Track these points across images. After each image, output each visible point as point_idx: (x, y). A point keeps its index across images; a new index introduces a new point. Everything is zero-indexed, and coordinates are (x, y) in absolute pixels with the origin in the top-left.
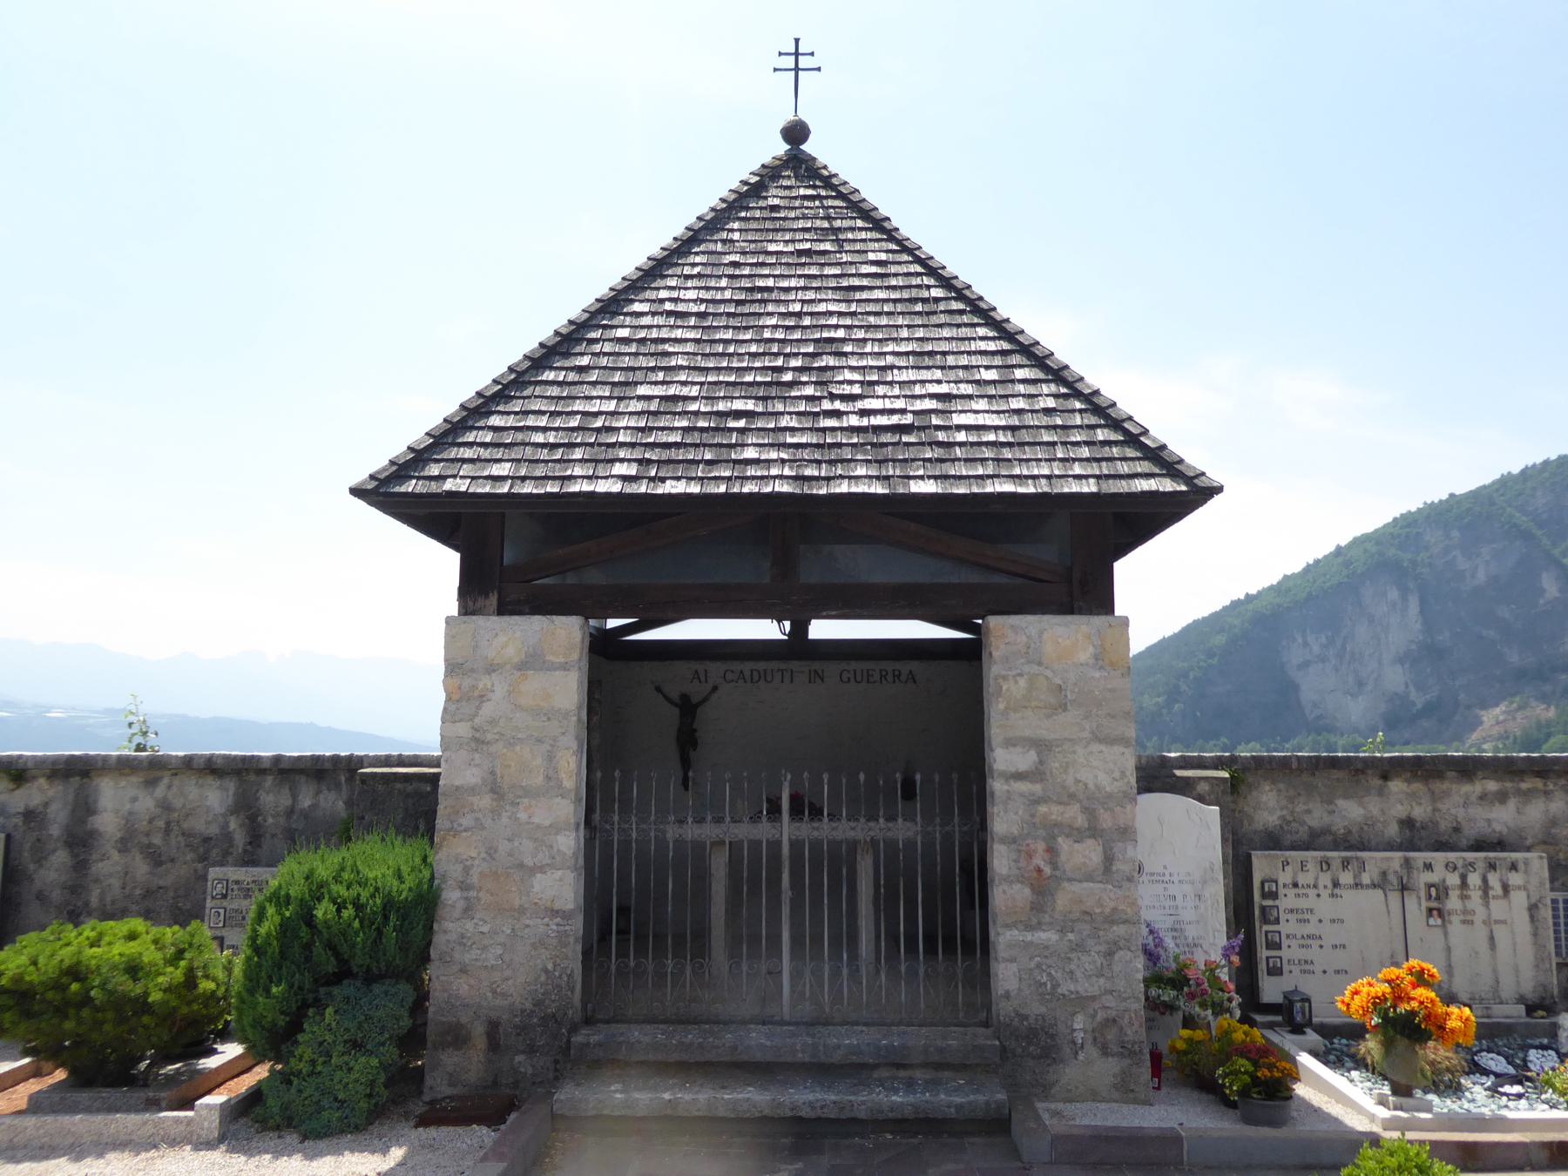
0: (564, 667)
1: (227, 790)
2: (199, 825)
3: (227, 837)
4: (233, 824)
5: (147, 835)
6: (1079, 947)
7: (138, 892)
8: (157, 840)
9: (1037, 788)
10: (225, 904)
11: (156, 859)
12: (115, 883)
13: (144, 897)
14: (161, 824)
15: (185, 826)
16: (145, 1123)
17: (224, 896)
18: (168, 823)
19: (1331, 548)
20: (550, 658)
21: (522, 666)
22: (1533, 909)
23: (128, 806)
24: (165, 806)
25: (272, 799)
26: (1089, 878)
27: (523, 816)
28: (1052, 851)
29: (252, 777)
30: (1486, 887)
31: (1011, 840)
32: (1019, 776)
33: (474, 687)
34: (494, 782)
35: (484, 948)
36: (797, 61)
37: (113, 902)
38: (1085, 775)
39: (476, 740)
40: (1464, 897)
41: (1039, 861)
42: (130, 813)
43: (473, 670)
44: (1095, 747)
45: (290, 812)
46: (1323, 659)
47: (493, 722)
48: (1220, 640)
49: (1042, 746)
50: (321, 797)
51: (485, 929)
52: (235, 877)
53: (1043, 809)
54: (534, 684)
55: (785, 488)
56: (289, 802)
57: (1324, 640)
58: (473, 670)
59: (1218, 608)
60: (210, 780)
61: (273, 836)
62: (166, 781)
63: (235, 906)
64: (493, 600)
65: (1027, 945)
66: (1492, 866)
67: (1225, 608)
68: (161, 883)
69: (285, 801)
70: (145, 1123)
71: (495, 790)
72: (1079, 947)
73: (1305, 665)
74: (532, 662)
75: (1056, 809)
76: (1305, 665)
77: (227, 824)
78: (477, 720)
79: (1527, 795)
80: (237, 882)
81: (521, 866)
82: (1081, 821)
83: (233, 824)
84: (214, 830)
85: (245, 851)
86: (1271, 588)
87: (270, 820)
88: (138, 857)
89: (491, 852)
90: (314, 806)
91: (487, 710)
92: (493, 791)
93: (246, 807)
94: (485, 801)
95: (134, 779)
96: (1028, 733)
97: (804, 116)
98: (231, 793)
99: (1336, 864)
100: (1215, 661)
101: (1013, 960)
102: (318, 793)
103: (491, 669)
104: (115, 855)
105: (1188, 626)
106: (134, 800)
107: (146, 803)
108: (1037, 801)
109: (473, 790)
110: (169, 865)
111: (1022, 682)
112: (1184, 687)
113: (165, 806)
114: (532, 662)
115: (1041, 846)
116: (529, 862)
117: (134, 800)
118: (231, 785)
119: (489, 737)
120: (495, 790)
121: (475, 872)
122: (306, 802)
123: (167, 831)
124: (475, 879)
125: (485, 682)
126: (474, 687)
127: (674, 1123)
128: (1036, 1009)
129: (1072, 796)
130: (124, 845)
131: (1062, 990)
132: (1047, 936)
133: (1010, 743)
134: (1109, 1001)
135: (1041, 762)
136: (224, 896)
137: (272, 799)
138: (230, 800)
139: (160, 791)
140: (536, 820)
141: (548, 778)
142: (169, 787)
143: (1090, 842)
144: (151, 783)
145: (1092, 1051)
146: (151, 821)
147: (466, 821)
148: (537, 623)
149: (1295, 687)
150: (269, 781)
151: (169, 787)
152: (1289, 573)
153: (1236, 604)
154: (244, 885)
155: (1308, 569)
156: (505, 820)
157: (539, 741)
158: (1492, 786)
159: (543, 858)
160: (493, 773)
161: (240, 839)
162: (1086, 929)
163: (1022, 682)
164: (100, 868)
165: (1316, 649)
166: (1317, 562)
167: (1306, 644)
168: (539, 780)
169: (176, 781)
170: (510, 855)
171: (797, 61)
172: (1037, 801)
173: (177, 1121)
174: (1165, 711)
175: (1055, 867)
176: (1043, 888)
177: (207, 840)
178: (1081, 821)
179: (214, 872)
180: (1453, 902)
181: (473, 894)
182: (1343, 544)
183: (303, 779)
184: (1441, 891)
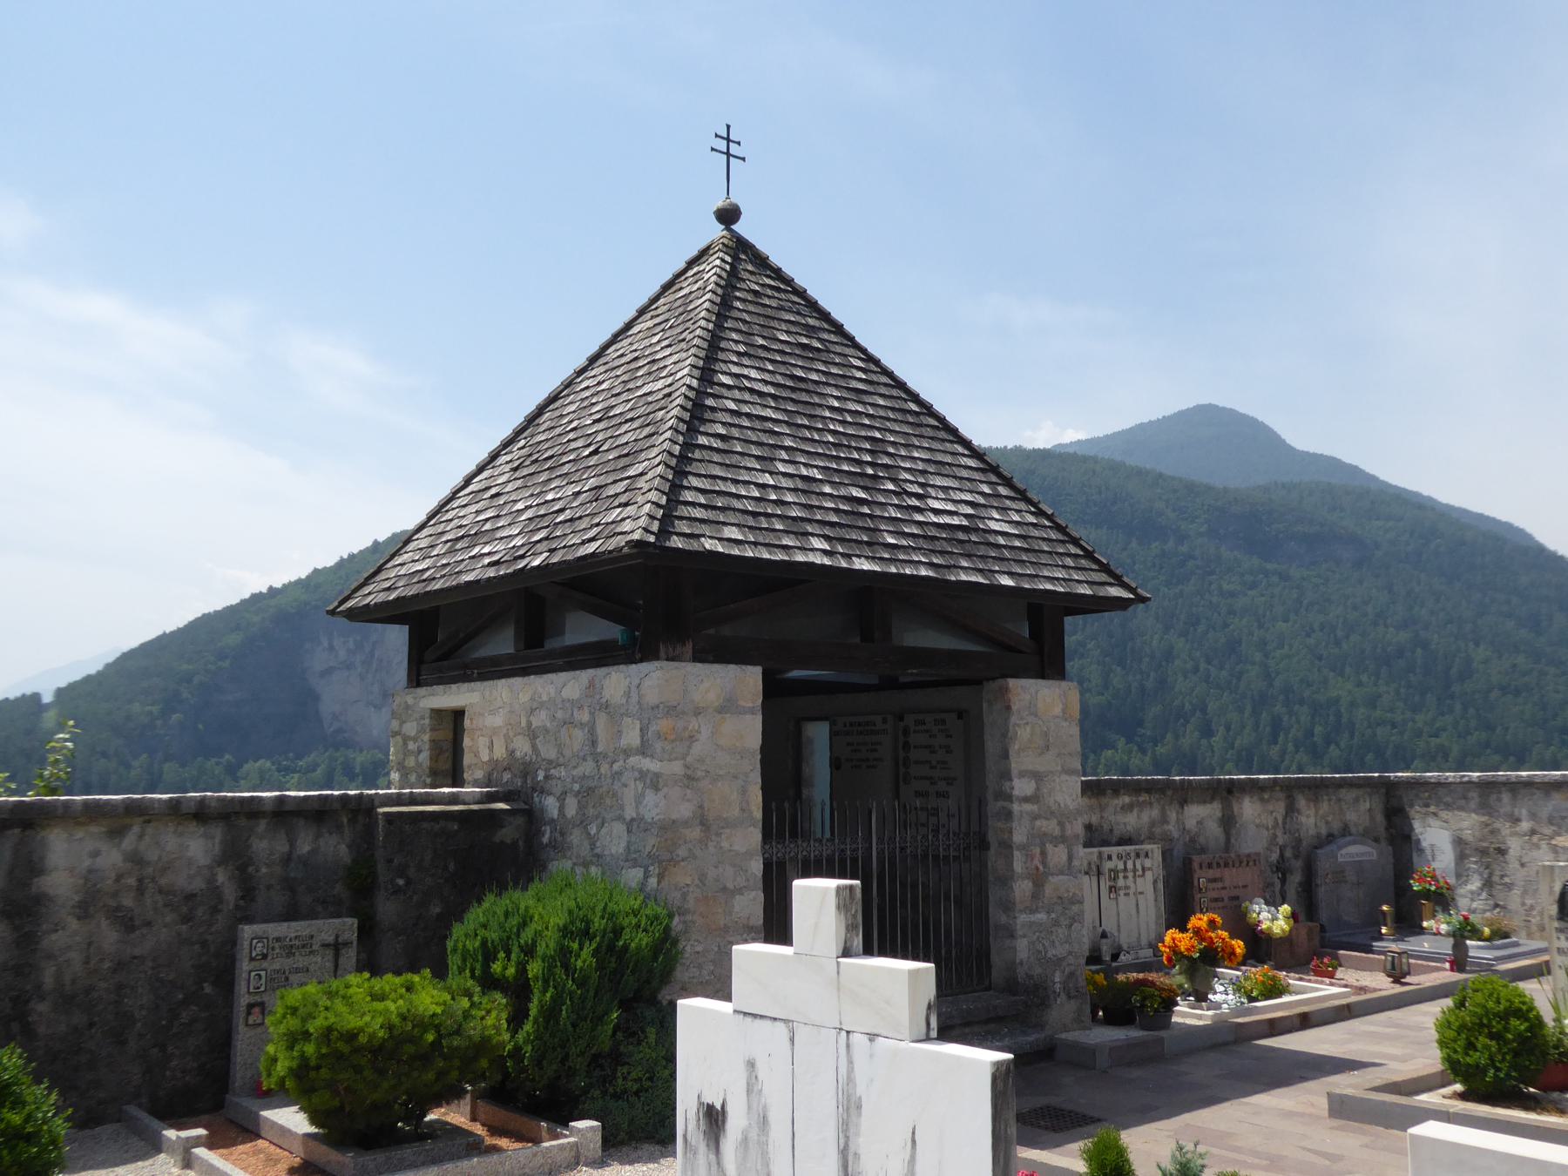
0: (752, 711)
1: (213, 838)
2: (182, 880)
3: (214, 891)
4: (221, 877)
5: (115, 895)
6: (1056, 923)
7: (107, 965)
8: (128, 901)
9: (1035, 808)
10: (265, 964)
11: (127, 923)
12: (76, 957)
13: (115, 971)
14: (132, 881)
15: (163, 881)
16: (535, 1155)
17: (265, 957)
18: (140, 880)
19: (369, 543)
20: (741, 703)
21: (721, 710)
22: (1155, 882)
23: (87, 863)
24: (136, 859)
25: (266, 846)
26: (1061, 873)
27: (725, 844)
28: (1043, 853)
29: (243, 822)
30: (1135, 870)
31: (1023, 847)
32: (1026, 799)
33: (686, 728)
34: (702, 816)
35: (700, 967)
36: (728, 147)
37: (73, 982)
38: (1059, 798)
39: (689, 777)
40: (1125, 877)
41: (1037, 862)
42: (90, 871)
43: (684, 713)
44: (1064, 777)
45: (287, 859)
46: (349, 666)
47: (701, 760)
48: (234, 639)
49: (1037, 776)
50: (322, 842)
51: (699, 948)
52: (276, 934)
53: (1038, 823)
54: (730, 725)
55: (923, 572)
56: (286, 848)
57: (351, 645)
58: (684, 713)
59: (235, 601)
60: (192, 826)
61: (269, 887)
62: (136, 829)
63: (277, 966)
64: (689, 647)
65: (1031, 924)
66: (1138, 855)
67: (243, 602)
68: (137, 952)
69: (282, 847)
70: (535, 1155)
71: (704, 823)
72: (1056, 923)
73: (328, 672)
74: (728, 707)
75: (1045, 823)
76: (328, 672)
77: (214, 875)
78: (689, 759)
79: (1141, 805)
80: (278, 939)
81: (724, 889)
82: (1057, 832)
83: (221, 877)
84: (198, 884)
85: (237, 907)
86: (299, 582)
87: (264, 870)
88: (104, 923)
89: (702, 878)
90: (314, 852)
91: (697, 749)
92: (702, 824)
93: (235, 856)
94: (695, 833)
95: (94, 829)
96: (1030, 767)
97: (734, 199)
98: (217, 841)
99: (1114, 857)
100: (226, 664)
101: (1024, 936)
102: (318, 836)
103: (698, 712)
104: (74, 924)
105: (197, 620)
106: (95, 854)
107: (111, 858)
108: (1035, 817)
109: (686, 823)
110: (144, 931)
111: (1028, 729)
112: (185, 695)
113: (136, 859)
114: (728, 707)
115: (1038, 850)
116: (730, 886)
117: (95, 854)
118: (218, 832)
119: (699, 774)
120: (704, 823)
121: (691, 898)
122: (304, 847)
123: (140, 890)
124: (691, 904)
125: (694, 724)
126: (686, 728)
127: (1375, 990)
128: (1038, 970)
129: (1052, 813)
130: (84, 910)
131: (1049, 955)
132: (1041, 916)
133: (1022, 775)
134: (1071, 960)
135: (1038, 789)
136: (265, 957)
137: (266, 846)
138: (217, 848)
139: (129, 842)
140: (736, 847)
141: (743, 810)
142: (141, 837)
143: (1062, 846)
144: (116, 833)
145: (1063, 998)
146: (119, 878)
147: (682, 852)
148: (732, 670)
149: (316, 698)
150: (262, 825)
151: (141, 837)
152: (320, 567)
153: (256, 598)
154: (287, 942)
155: (342, 563)
156: (712, 849)
157: (735, 777)
158: (1127, 799)
159: (741, 881)
160: (701, 807)
161: (230, 894)
162: (1059, 908)
163: (1028, 729)
164: (54, 941)
165: (342, 654)
166: (352, 557)
167: (331, 648)
168: (736, 812)
169: (150, 830)
170: (717, 881)
171: (728, 147)
172: (1035, 817)
173: (561, 1147)
174: (159, 722)
175: (1044, 863)
176: (1039, 881)
177: (190, 897)
178: (1057, 832)
179: (248, 931)
180: (1121, 882)
181: (689, 917)
182: (381, 540)
183: (302, 822)
184: (1115, 871)
